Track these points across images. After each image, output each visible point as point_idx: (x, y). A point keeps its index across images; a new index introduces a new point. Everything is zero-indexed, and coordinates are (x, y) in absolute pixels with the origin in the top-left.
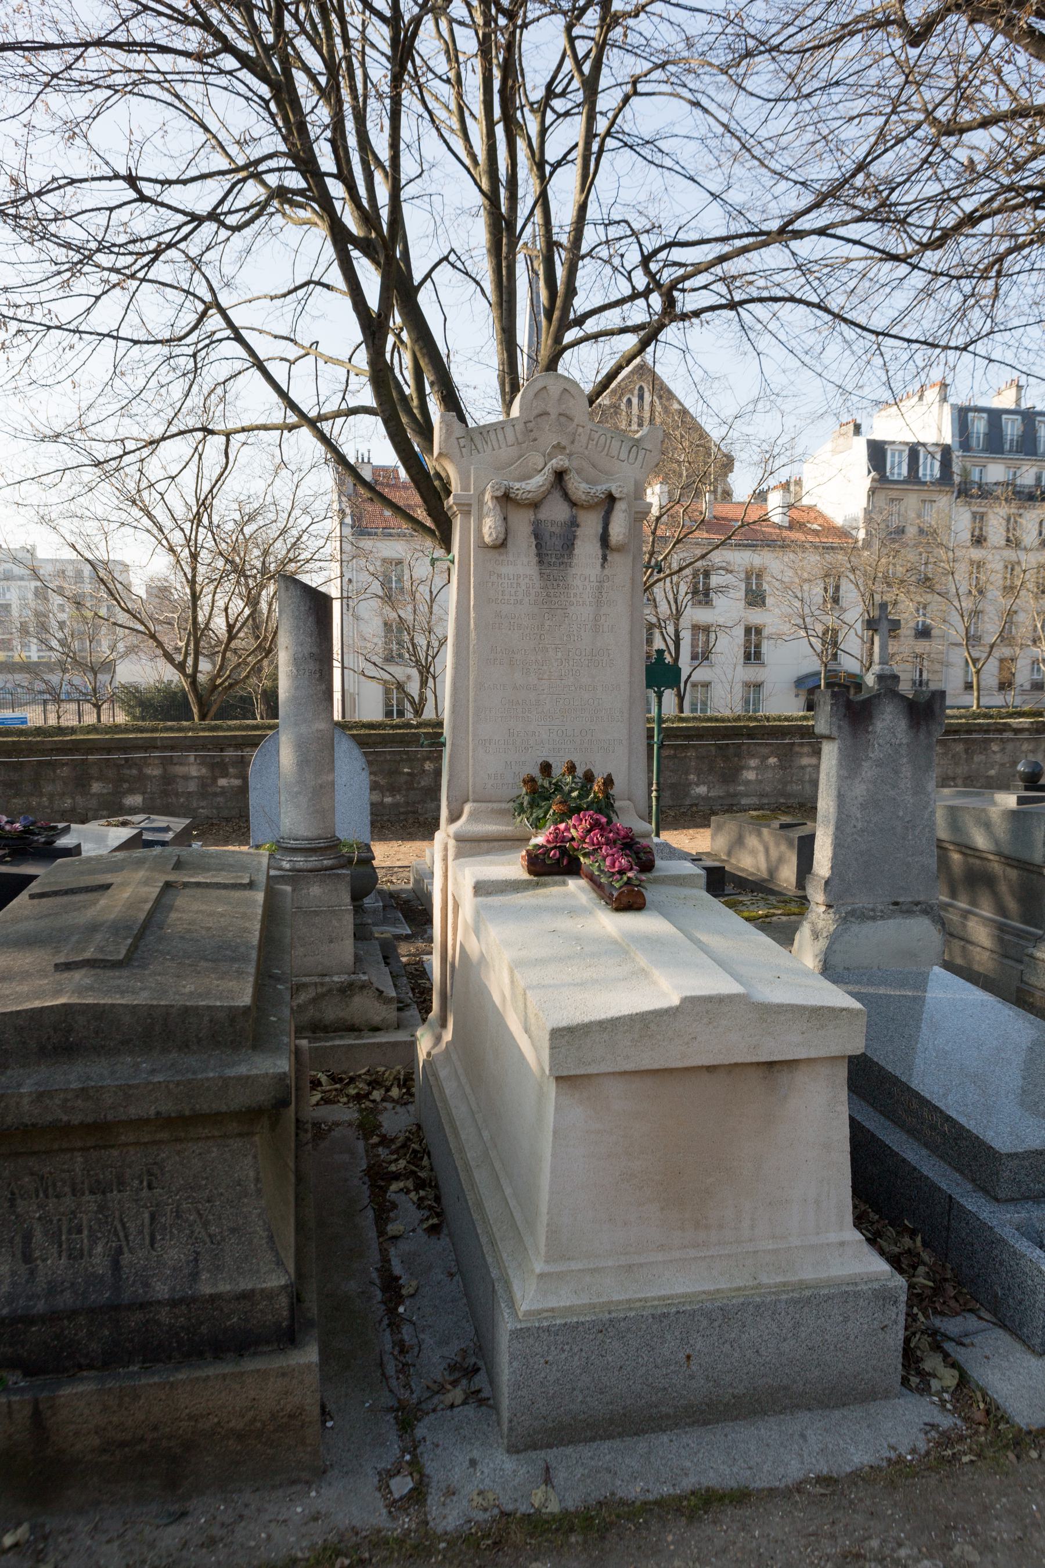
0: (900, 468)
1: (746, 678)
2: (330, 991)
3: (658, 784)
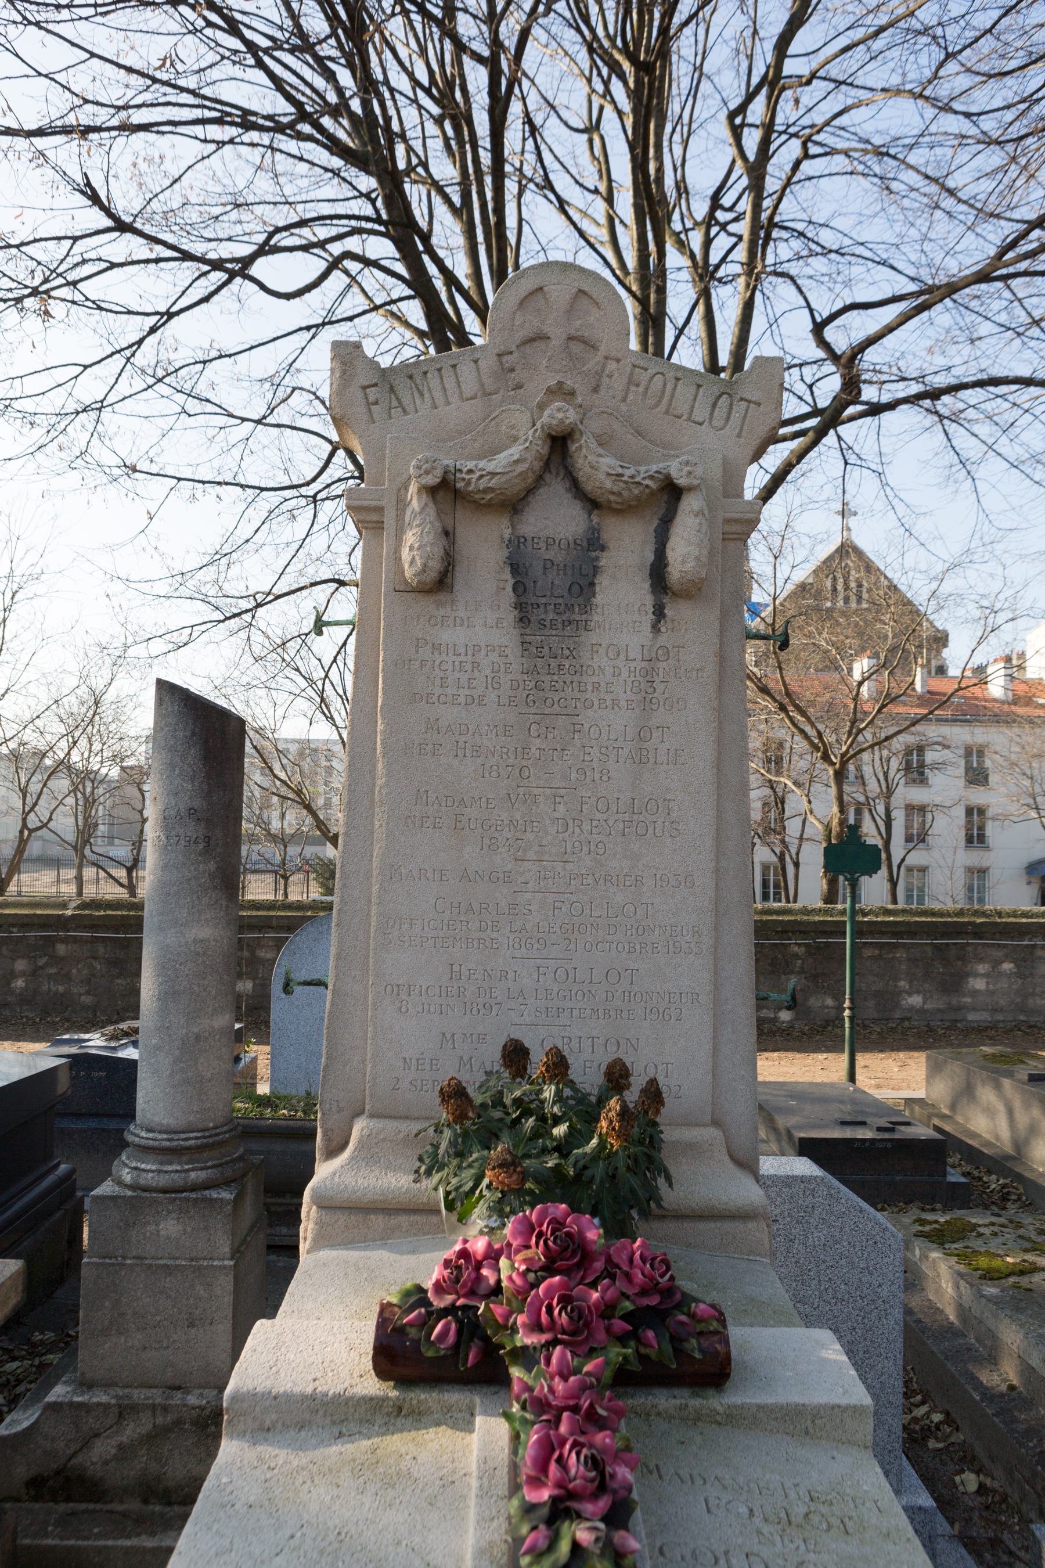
1: (969, 863)
2: (179, 1422)
3: (852, 1000)
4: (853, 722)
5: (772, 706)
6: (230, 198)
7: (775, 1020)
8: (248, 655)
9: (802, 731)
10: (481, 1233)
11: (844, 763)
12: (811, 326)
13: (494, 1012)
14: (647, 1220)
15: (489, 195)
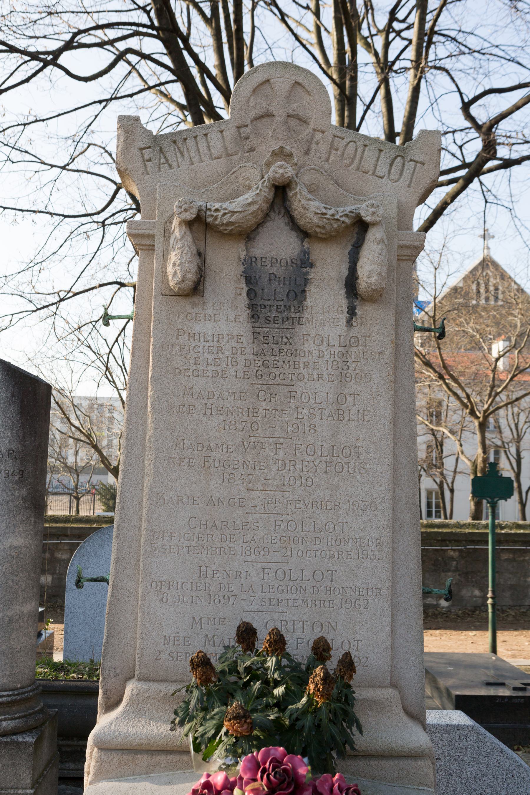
3: (493, 592)
4: (493, 387)
5: (433, 376)
6: (45, 9)
7: (437, 606)
8: (53, 336)
9: (455, 394)
10: (220, 769)
11: (486, 417)
12: (460, 105)
13: (231, 602)
14: (344, 759)
15: (231, 9)
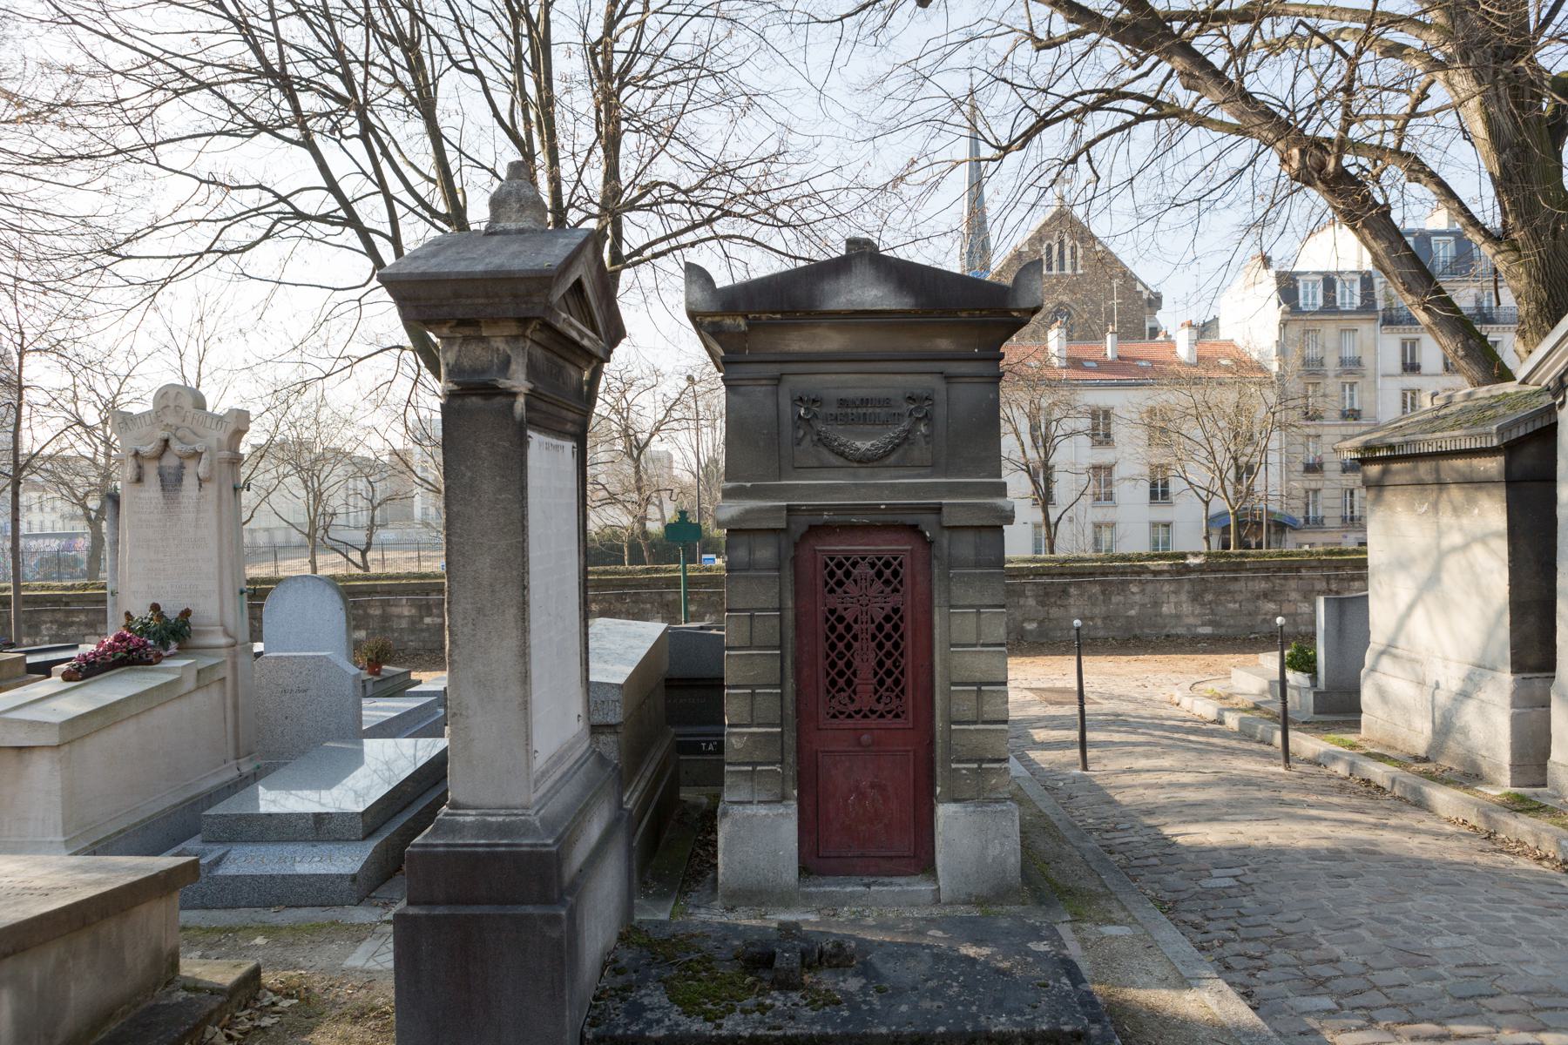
0: (1314, 297)
